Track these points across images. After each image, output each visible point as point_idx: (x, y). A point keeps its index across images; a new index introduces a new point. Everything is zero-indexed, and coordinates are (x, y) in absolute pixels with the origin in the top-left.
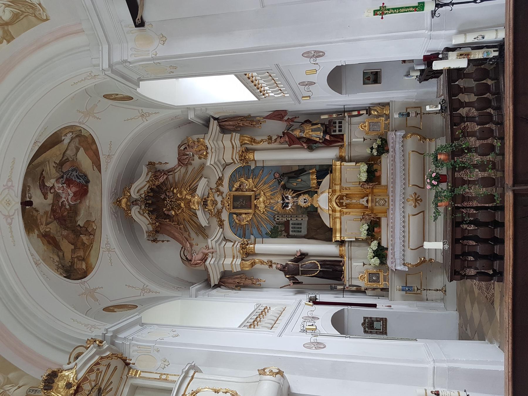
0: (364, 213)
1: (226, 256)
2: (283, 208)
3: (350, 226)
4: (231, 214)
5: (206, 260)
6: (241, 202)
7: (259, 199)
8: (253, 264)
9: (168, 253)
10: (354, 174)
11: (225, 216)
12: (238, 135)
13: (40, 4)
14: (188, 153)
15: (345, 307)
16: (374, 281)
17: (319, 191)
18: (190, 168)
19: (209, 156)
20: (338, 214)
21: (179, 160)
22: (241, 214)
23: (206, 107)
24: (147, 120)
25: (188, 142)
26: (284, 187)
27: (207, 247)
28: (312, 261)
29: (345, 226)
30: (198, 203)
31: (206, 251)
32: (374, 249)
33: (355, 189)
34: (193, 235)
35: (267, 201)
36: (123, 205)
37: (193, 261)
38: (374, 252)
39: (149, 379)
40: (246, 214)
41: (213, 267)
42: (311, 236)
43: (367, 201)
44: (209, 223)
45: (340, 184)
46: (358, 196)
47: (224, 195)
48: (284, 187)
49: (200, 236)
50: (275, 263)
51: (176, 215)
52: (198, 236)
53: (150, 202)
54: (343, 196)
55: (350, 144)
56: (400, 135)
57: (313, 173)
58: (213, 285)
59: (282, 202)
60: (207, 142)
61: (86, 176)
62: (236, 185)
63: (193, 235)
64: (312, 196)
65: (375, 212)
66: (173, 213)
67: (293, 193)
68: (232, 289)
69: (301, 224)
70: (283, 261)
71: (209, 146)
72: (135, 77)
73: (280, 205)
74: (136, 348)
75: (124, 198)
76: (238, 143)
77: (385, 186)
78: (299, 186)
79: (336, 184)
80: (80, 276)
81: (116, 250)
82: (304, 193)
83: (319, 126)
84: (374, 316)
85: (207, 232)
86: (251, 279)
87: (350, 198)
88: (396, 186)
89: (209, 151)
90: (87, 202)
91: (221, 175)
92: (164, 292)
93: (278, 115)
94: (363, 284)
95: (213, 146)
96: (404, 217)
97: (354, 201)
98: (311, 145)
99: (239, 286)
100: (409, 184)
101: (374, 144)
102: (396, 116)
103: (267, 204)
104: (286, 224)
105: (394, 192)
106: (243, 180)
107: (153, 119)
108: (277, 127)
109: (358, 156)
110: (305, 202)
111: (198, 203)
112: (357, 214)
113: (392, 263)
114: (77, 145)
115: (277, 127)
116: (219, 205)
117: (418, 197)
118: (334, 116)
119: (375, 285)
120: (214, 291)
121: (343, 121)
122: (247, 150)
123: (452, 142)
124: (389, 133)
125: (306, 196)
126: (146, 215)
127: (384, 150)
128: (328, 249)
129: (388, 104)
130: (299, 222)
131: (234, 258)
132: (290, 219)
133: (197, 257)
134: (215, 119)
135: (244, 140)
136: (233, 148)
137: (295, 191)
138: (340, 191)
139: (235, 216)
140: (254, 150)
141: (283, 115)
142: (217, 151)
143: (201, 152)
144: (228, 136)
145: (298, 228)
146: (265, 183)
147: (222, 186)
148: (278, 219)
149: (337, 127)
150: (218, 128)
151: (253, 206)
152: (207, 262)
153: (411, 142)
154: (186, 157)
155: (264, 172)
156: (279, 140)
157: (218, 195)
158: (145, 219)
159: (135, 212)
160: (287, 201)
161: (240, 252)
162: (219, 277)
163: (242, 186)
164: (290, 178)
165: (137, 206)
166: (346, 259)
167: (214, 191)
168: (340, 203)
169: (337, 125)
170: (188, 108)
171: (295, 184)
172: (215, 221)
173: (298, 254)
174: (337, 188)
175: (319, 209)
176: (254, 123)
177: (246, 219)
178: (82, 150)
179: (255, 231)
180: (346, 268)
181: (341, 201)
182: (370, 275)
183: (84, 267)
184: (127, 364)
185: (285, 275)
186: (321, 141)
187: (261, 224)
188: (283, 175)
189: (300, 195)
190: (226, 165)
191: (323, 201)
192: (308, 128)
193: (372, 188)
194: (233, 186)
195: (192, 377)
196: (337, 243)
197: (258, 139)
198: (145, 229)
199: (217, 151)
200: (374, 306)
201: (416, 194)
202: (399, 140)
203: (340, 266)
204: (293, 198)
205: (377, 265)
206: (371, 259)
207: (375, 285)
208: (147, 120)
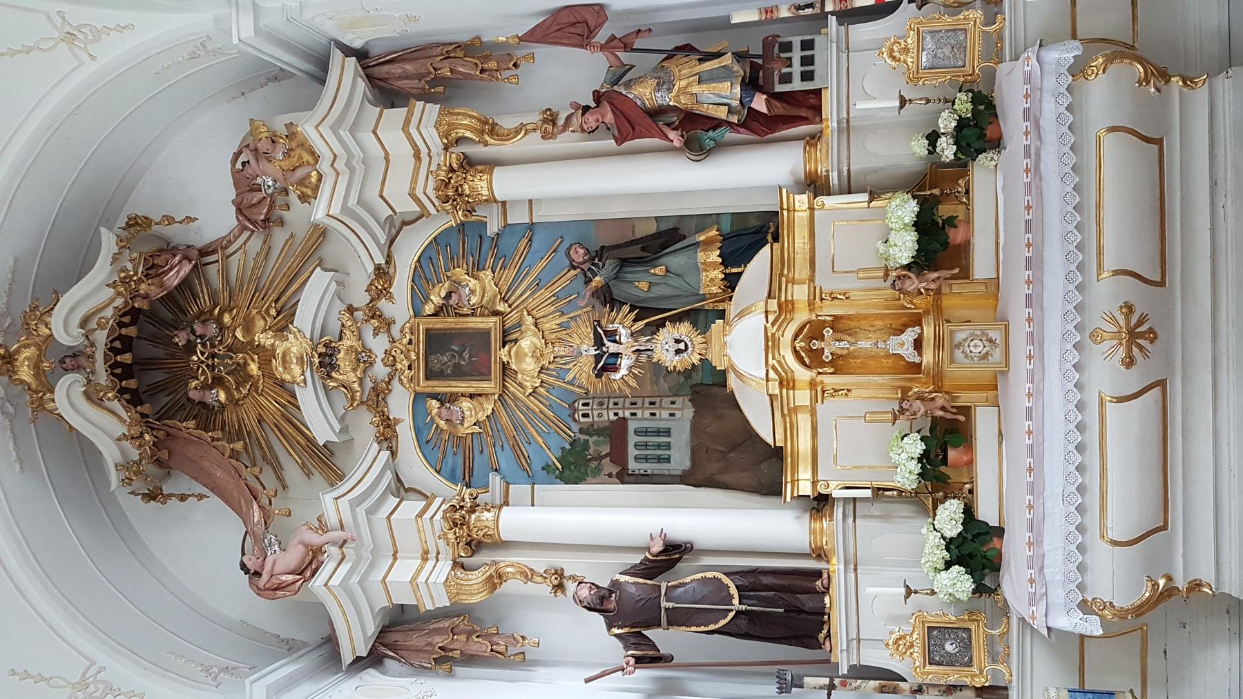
0: (905, 390)
2: (599, 376)
3: (852, 438)
4: (420, 398)
6: (454, 353)
7: (516, 341)
8: (495, 580)
9: (201, 539)
10: (860, 241)
11: (400, 404)
12: (433, 110)
16: (950, 660)
17: (732, 309)
18: (279, 237)
20: (802, 397)
21: (239, 211)
22: (453, 398)
24: (93, 58)
28: (710, 575)
31: (315, 539)
32: (949, 535)
35: (547, 348)
37: (265, 577)
38: (949, 543)
40: (471, 396)
43: (918, 344)
44: (344, 430)
45: (812, 280)
46: (879, 324)
47: (395, 330)
49: (318, 478)
50: (572, 578)
52: (309, 475)
54: (822, 324)
55: (846, 128)
56: (1058, 62)
57: (708, 243)
58: (347, 658)
59: (593, 352)
63: (292, 472)
66: (222, 396)
67: (635, 321)
68: (421, 670)
69: (668, 432)
70: (603, 571)
75: (26, 346)
76: (436, 143)
77: (985, 283)
78: (658, 291)
79: (794, 282)
82: (677, 319)
83: (727, 60)
85: (340, 461)
86: (488, 636)
87: (849, 332)
88: (1047, 280)
89: (324, 166)
96: (1080, 407)
97: (864, 344)
98: (696, 133)
99: (445, 661)
100: (1100, 267)
101: (945, 114)
103: (546, 362)
104: (616, 432)
106: (460, 273)
108: (572, 74)
109: (876, 171)
110: (678, 352)
111: (300, 360)
112: (871, 393)
113: (1033, 601)
115: (572, 74)
117: (1140, 323)
119: (953, 676)
121: (818, 40)
122: (468, 163)
124: (1002, 69)
125: (684, 329)
127: (982, 136)
130: (662, 425)
131: (425, 559)
132: (627, 414)
133: (283, 560)
134: (348, 51)
135: (453, 127)
137: (642, 311)
138: (811, 305)
139: (435, 403)
140: (491, 164)
141: (592, 23)
142: (360, 168)
143: (300, 173)
145: (659, 446)
146: (538, 285)
147: (390, 298)
149: (796, 62)
150: (362, 85)
151: (496, 370)
153: (1108, 92)
155: (535, 244)
156: (576, 121)
157: (376, 333)
158: (115, 420)
159: (68, 395)
160: (613, 348)
161: (444, 536)
163: (454, 296)
164: (624, 262)
166: (836, 566)
168: (810, 351)
169: (796, 55)
171: (644, 286)
172: (365, 425)
173: (657, 547)
174: (800, 293)
176: (492, 65)
177: (471, 414)
179: (505, 459)
180: (837, 603)
181: (816, 345)
182: (936, 634)
185: (609, 627)
186: (734, 119)
188: (598, 255)
189: (661, 324)
190: (397, 226)
191: (744, 346)
192: (685, 73)
194: (427, 299)
196: (801, 502)
197: (508, 123)
198: (110, 453)
199: (360, 168)
201: (1129, 308)
202: (1054, 84)
203: (814, 591)
205: (964, 597)
206: (937, 570)
207: (953, 676)
208: (93, 58)
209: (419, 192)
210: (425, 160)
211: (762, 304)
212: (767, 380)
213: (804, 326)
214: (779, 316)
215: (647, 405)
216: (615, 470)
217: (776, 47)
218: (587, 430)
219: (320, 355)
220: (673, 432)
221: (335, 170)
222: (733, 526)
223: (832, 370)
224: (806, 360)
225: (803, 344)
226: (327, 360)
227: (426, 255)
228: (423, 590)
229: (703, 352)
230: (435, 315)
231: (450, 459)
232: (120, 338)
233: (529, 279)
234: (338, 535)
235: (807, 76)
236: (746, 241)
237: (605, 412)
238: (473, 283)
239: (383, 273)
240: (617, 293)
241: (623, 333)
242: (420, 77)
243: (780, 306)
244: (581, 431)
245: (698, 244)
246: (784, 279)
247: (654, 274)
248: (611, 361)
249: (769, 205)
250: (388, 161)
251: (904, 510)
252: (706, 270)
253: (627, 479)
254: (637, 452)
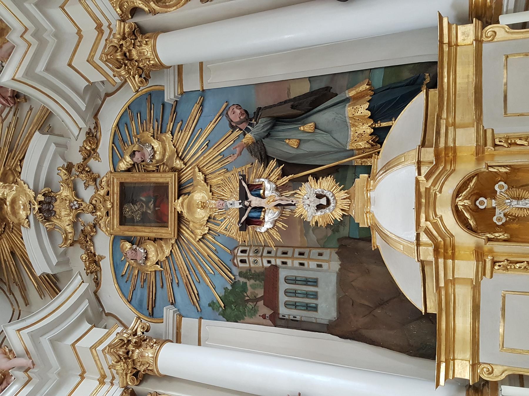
4: (116, 240)
7: (189, 193)
11: (103, 244)
17: (378, 163)
20: (466, 268)
40: (155, 240)
45: (479, 119)
57: (357, 98)
67: (284, 174)
69: (315, 282)
78: (307, 148)
122: (139, 31)
125: (327, 185)
132: (279, 262)
137: (289, 167)
138: (479, 153)
139: (128, 245)
145: (307, 295)
147: (97, 158)
148: (243, 261)
155: (206, 110)
160: (255, 201)
164: (278, 121)
168: (475, 211)
171: (294, 143)
174: (465, 139)
179: (181, 294)
181: (484, 203)
189: (305, 179)
191: (389, 202)
210: (107, 32)
211: (414, 154)
212: (418, 244)
213: (470, 180)
214: (437, 166)
215: (296, 255)
216: (268, 312)
218: (246, 274)
219: (40, 203)
220: (320, 283)
221: (26, 41)
223: (506, 236)
224: (472, 222)
225: (467, 202)
226: (45, 207)
227: (123, 121)
229: (346, 208)
230: (129, 170)
231: (139, 291)
233: (201, 140)
234: (24, 361)
236: (398, 93)
237: (259, 259)
238: (156, 145)
239: (93, 137)
240: (270, 151)
241: (268, 187)
243: (437, 156)
244: (241, 274)
245: (347, 100)
246: (443, 122)
247: (304, 132)
248: (255, 214)
249: (424, 53)
250: (81, 37)
252: (354, 125)
253: (279, 322)
254: (287, 299)
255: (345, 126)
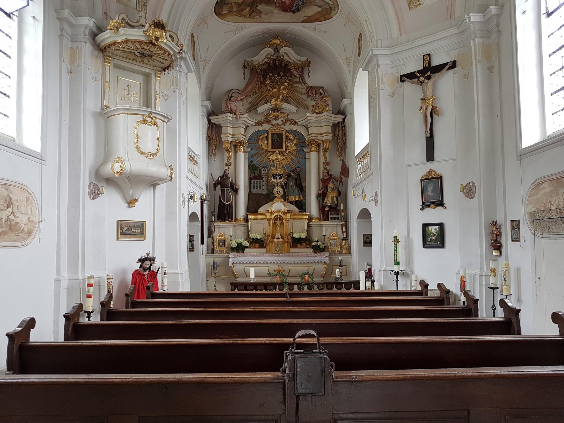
1: (234, 129)
3: (259, 226)
4: (267, 132)
5: (230, 112)
8: (228, 151)
9: (234, 79)
11: (266, 127)
12: (330, 138)
13: (420, 4)
14: (317, 96)
15: (200, 222)
16: (219, 244)
17: (286, 203)
18: (305, 97)
19: (314, 115)
20: (268, 217)
22: (267, 140)
23: (352, 114)
25: (326, 97)
26: (289, 176)
27: (241, 114)
29: (259, 222)
30: (276, 104)
31: (238, 113)
33: (288, 228)
34: (250, 99)
35: (278, 161)
36: (275, 41)
38: (241, 244)
39: (155, 87)
40: (268, 144)
41: (225, 118)
42: (251, 196)
47: (282, 126)
48: (289, 176)
50: (229, 168)
51: (266, 85)
53: (277, 64)
55: (321, 226)
57: (300, 198)
58: (210, 118)
60: (325, 113)
61: (298, 11)
62: (291, 137)
63: (250, 99)
64: (282, 197)
65: (270, 244)
66: (268, 82)
70: (231, 174)
71: (322, 115)
72: (370, 69)
73: (275, 172)
74: (175, 75)
76: (324, 138)
78: (290, 187)
80: (217, 11)
81: (237, 35)
82: (284, 191)
83: (336, 202)
84: (195, 242)
89: (318, 115)
90: (277, 11)
91: (299, 123)
92: (204, 78)
93: (345, 171)
94: (216, 235)
95: (322, 118)
98: (322, 196)
99: (209, 140)
102: (340, 258)
105: (285, 256)
107: (345, 67)
108: (336, 170)
111: (276, 104)
114: (324, 7)
115: (336, 170)
116: (274, 122)
118: (343, 214)
119: (216, 244)
120: (206, 120)
123: (316, 284)
124: (329, 253)
125: (282, 193)
126: (266, 60)
127: (316, 250)
128: (241, 210)
129: (350, 253)
133: (233, 105)
136: (320, 134)
140: (318, 151)
143: (317, 108)
144: (330, 129)
151: (274, 150)
152: (229, 114)
153: (321, 268)
154: (314, 94)
157: (282, 121)
159: (269, 51)
160: (278, 178)
162: (216, 123)
164: (296, 179)
165: (273, 52)
166: (234, 223)
167: (286, 117)
169: (336, 216)
170: (352, 99)
171: (291, 184)
172: (262, 118)
173: (237, 187)
174: (288, 216)
175: (272, 203)
178: (320, 9)
179: (254, 152)
180: (227, 223)
182: (223, 241)
183: (224, 12)
184: (164, 70)
187: (259, 156)
188: (299, 174)
189: (283, 188)
191: (278, 205)
193: (288, 242)
194: (289, 134)
195: (164, 121)
197: (327, 154)
198: (254, 59)
200: (202, 243)
201: (284, 271)
202: (322, 259)
204: (281, 182)
207: (216, 244)
209: (312, 135)
217: (338, 212)
222: (242, 201)
228: (225, 135)
232: (282, 61)
235: (331, 218)
242: (338, 134)
251: (246, 236)
255: (294, 195)
